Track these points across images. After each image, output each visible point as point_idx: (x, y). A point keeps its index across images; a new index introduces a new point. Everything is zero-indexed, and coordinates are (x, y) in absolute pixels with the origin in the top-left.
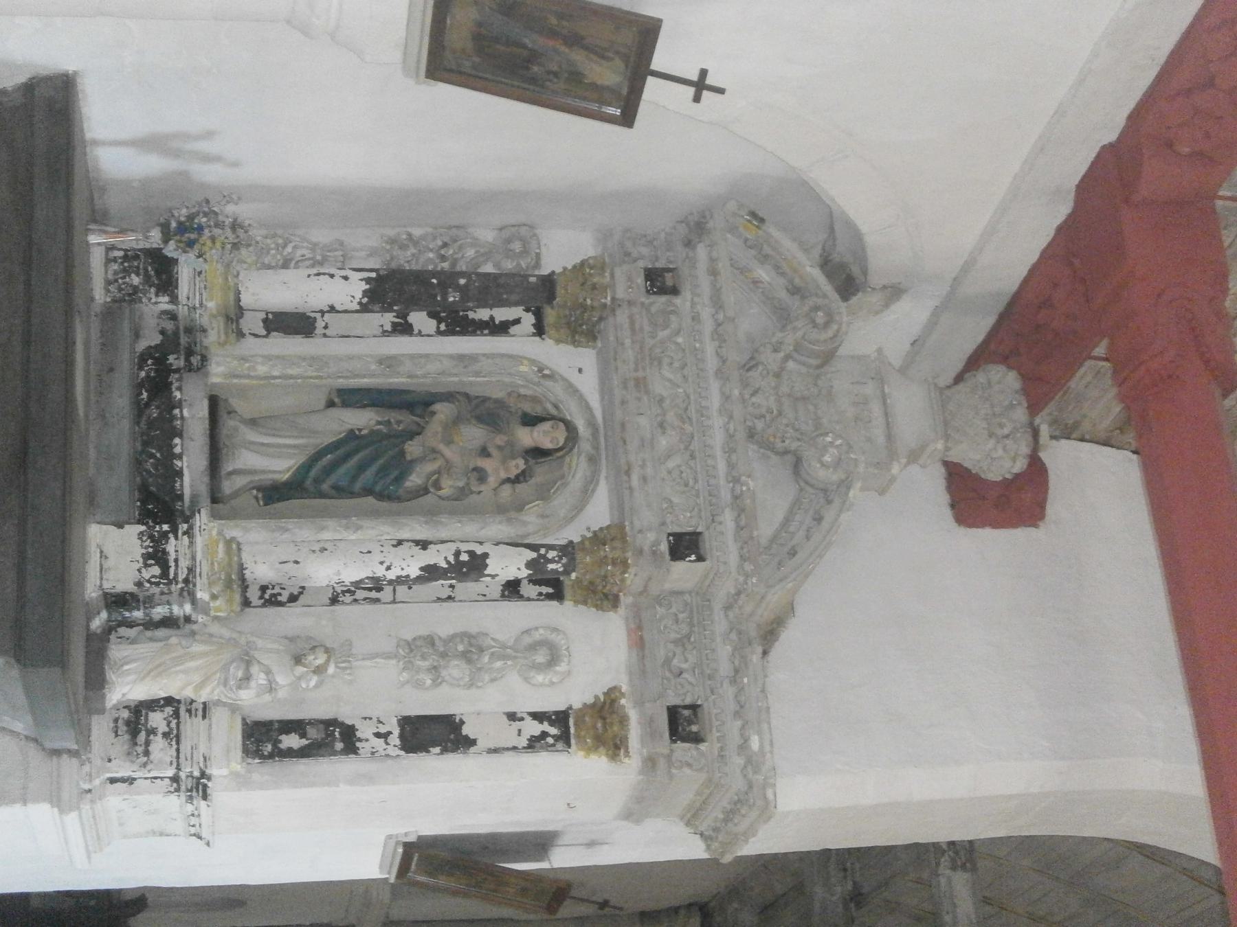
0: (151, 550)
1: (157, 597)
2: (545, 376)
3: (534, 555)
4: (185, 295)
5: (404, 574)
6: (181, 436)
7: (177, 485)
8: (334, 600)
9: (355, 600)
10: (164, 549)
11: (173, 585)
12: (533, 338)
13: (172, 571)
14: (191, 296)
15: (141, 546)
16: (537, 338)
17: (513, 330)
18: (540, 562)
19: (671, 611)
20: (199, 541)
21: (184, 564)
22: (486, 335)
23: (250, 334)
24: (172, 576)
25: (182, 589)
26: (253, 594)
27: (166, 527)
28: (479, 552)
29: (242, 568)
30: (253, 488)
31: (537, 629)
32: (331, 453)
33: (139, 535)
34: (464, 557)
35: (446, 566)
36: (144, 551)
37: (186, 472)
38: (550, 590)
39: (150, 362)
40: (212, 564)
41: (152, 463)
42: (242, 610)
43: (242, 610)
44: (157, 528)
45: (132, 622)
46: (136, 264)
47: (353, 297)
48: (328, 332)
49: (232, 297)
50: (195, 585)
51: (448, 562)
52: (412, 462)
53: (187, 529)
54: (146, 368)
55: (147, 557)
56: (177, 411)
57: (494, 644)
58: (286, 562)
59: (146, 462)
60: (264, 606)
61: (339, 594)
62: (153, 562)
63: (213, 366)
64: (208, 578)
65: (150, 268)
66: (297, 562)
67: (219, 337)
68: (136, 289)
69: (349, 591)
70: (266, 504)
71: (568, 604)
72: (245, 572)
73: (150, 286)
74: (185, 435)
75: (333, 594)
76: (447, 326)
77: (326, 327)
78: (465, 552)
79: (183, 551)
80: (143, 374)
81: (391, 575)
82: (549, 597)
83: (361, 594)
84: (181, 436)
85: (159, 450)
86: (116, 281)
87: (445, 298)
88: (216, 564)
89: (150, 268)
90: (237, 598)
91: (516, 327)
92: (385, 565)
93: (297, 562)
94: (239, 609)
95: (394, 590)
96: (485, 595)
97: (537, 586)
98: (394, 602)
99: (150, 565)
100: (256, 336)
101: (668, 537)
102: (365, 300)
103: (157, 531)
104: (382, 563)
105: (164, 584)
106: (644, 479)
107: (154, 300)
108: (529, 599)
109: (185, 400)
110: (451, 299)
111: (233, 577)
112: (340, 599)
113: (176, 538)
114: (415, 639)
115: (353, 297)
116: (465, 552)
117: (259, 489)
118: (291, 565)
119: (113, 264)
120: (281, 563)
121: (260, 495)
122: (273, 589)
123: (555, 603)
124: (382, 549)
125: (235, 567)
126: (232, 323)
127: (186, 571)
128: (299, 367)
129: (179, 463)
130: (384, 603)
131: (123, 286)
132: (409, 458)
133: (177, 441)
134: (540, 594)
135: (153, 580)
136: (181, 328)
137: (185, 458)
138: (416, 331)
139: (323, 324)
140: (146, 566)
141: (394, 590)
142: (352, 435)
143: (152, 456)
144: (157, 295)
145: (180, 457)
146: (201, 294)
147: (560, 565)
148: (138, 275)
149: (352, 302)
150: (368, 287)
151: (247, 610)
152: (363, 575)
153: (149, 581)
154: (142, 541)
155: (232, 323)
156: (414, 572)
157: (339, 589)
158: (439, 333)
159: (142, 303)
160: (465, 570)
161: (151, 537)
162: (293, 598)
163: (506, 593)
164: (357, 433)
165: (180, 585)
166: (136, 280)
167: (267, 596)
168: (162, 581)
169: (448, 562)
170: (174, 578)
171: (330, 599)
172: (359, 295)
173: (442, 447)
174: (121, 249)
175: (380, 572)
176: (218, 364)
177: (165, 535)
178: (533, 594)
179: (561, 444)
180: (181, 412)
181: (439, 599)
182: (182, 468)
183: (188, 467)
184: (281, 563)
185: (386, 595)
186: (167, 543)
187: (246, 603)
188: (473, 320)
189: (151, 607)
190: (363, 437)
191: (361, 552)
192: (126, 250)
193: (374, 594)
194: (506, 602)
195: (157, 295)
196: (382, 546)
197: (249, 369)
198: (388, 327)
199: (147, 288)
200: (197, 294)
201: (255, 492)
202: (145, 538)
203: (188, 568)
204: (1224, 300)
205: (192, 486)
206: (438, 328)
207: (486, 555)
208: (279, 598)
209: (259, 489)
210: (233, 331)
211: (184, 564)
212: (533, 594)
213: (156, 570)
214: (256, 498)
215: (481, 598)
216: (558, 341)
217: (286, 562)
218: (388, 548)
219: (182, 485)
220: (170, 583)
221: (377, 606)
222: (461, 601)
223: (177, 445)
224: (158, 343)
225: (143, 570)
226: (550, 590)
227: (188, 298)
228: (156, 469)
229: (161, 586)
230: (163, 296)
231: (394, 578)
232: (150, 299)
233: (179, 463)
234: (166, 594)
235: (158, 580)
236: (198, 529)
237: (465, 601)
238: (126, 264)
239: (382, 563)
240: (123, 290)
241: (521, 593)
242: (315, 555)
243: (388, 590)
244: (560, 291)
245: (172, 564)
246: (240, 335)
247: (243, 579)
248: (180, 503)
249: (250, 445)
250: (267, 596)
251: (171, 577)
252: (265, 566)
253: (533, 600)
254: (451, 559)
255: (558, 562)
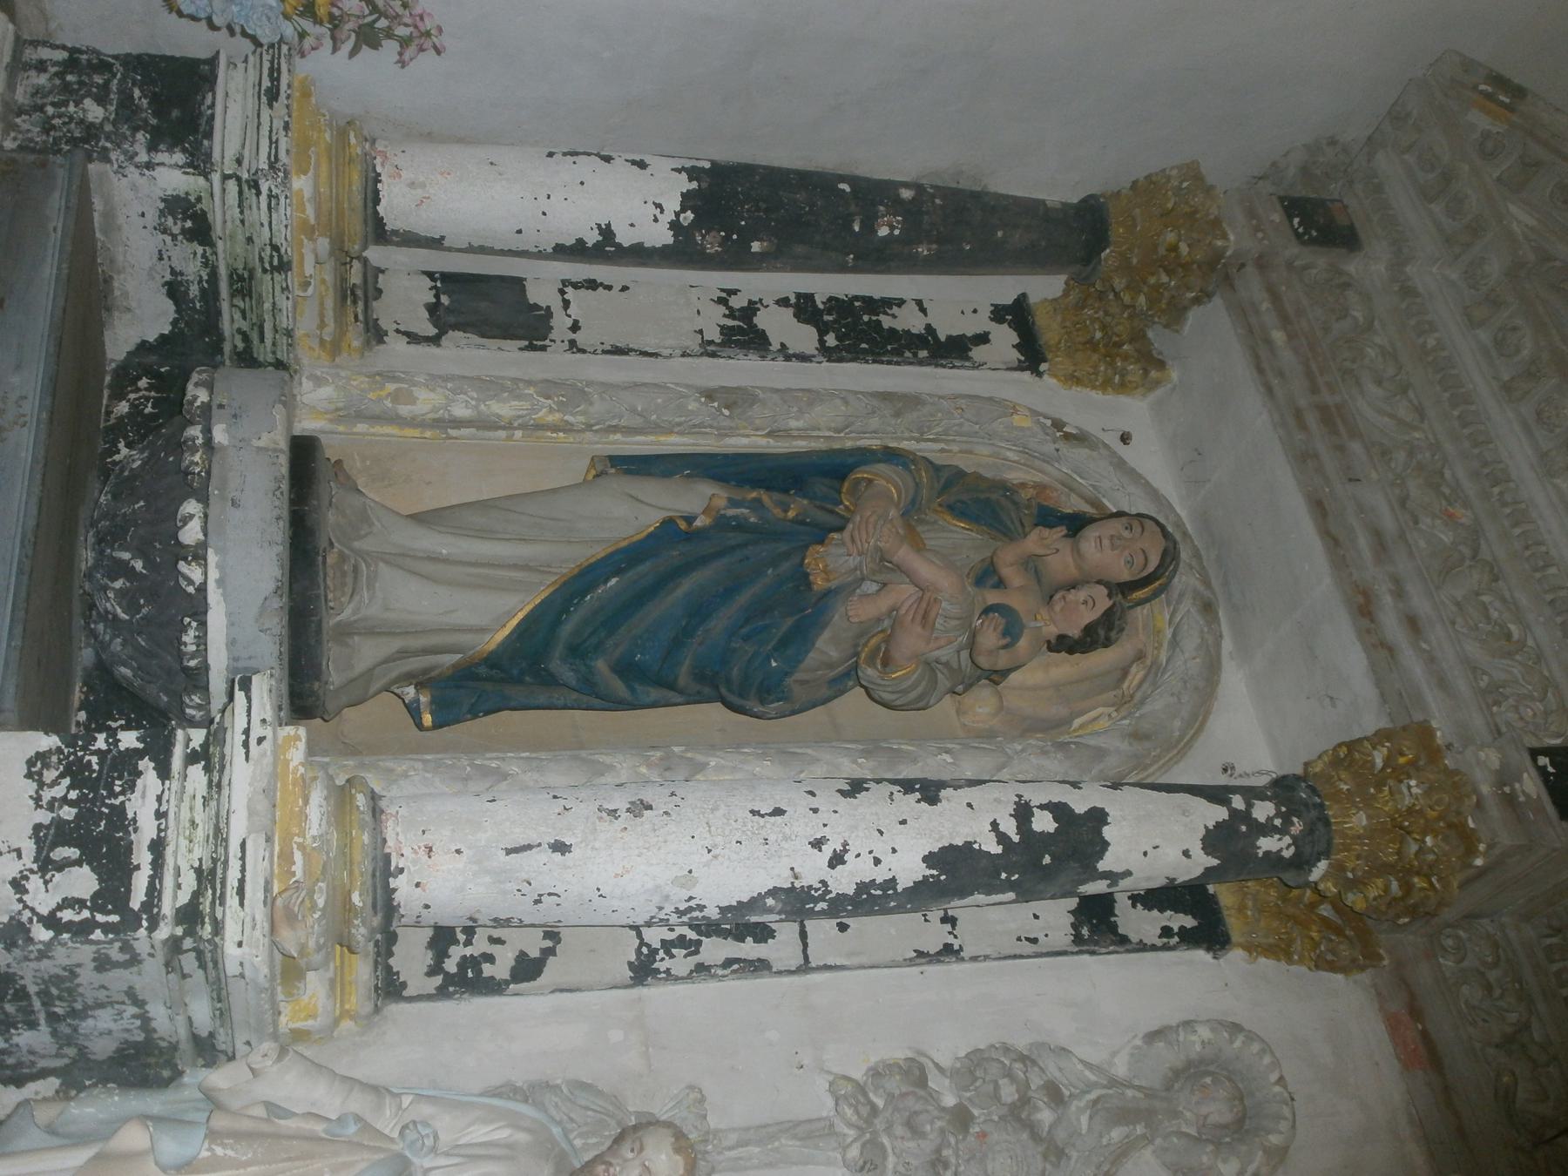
0: (68, 813)
1: (87, 976)
2: (1067, 436)
3: (1221, 813)
4: (231, 153)
5: (880, 875)
6: (204, 500)
7: (189, 637)
8: (643, 970)
9: (701, 968)
10: (120, 811)
11: (142, 932)
12: (1017, 374)
13: (140, 882)
14: (246, 153)
15: (37, 800)
16: (1026, 375)
17: (977, 353)
18: (1237, 831)
19: (1465, 964)
20: (242, 776)
21: (185, 856)
22: (921, 363)
23: (398, 331)
24: (137, 898)
25: (174, 945)
26: (411, 958)
27: (129, 740)
28: (1080, 808)
29: (384, 870)
30: (408, 678)
31: (1188, 1024)
32: (618, 572)
33: (31, 763)
34: (1044, 823)
35: (998, 850)
36: (44, 817)
37: (214, 596)
38: (1189, 922)
39: (143, 383)
40: (286, 858)
41: (121, 593)
42: (377, 1010)
43: (377, 1010)
44: (101, 742)
45: (20, 1064)
46: (98, 79)
47: (658, 206)
48: (579, 337)
49: (356, 179)
50: (218, 928)
51: (1002, 838)
52: (828, 593)
53: (205, 745)
54: (132, 396)
55: (48, 838)
56: (195, 432)
57: (1093, 1078)
58: (529, 847)
59: (105, 588)
60: (442, 993)
61: (656, 951)
62: (73, 853)
63: (307, 384)
64: (270, 901)
65: (137, 93)
66: (560, 847)
67: (322, 325)
68: (91, 132)
69: (682, 942)
70: (437, 725)
71: (1236, 955)
72: (393, 883)
73: (135, 129)
74: (214, 492)
75: (639, 951)
76: (837, 338)
77: (575, 327)
78: (1042, 807)
79: (185, 814)
80: (123, 408)
81: (843, 882)
82: (1189, 938)
83: (715, 950)
84: (204, 500)
85: (140, 552)
86: (41, 109)
87: (869, 226)
88: (298, 856)
89: (137, 93)
90: (362, 971)
91: (983, 348)
92: (828, 850)
93: (560, 847)
94: (368, 1007)
95: (803, 935)
96: (1034, 941)
97: (1155, 912)
98: (805, 967)
99: (61, 866)
100: (413, 338)
101: (1534, 760)
102: (688, 217)
103: (98, 752)
104: (818, 844)
105: (106, 928)
106: (1413, 624)
107: (143, 157)
108: (1142, 947)
109: (221, 406)
110: (883, 232)
111: (356, 898)
112: (662, 966)
113: (164, 772)
114: (876, 1073)
115: (658, 206)
116: (1042, 807)
117: (422, 680)
118: (544, 856)
119: (33, 73)
120: (509, 852)
121: (424, 699)
122: (468, 943)
123: (1201, 955)
124: (815, 802)
125: (363, 865)
126: (355, 302)
127: (189, 882)
128: (519, 397)
129: (195, 573)
130: (780, 973)
131: (56, 121)
132: (819, 583)
133: (191, 507)
134: (1166, 932)
135: (67, 915)
136: (223, 272)
137: (212, 557)
138: (775, 346)
139: (569, 322)
140: (46, 865)
141: (803, 935)
142: (670, 532)
143: (125, 570)
144: (152, 147)
145: (198, 554)
146: (274, 143)
147: (1287, 840)
148: (101, 100)
149: (656, 220)
150: (694, 185)
151: (395, 1009)
152: (762, 884)
153: (51, 921)
154: (41, 785)
155: (355, 302)
156: (909, 868)
157: (654, 936)
158: (828, 353)
159: (109, 161)
160: (1047, 860)
161: (75, 772)
162: (527, 969)
163: (1085, 931)
164: (683, 525)
165: (163, 932)
166: (94, 112)
167: (451, 966)
168: (100, 918)
169: (1002, 838)
170: (148, 906)
171: (630, 964)
172: (673, 204)
173: (904, 554)
174: (64, 47)
175: (813, 870)
176: (319, 382)
177: (124, 766)
178: (1151, 934)
179: (1151, 568)
180: (207, 431)
181: (920, 954)
182: (202, 589)
183: (220, 582)
184: (509, 852)
185: (782, 947)
186: (130, 787)
187: (390, 988)
188: (892, 331)
189: (73, 1013)
190: (700, 534)
191: (753, 812)
192: (73, 51)
193: (749, 949)
194: (1086, 957)
195: (152, 147)
196: (812, 794)
197: (396, 397)
198: (714, 335)
199: (125, 129)
200: (265, 143)
201: (410, 692)
202: (50, 775)
203: (199, 871)
204: (139, 1042)
205: (231, 643)
206: (822, 342)
207: (1098, 817)
208: (487, 970)
209: (422, 680)
210: (356, 317)
211: (185, 856)
212: (1151, 934)
213: (83, 882)
214: (413, 710)
215: (1029, 948)
216: (1073, 379)
217: (529, 847)
218: (827, 799)
219: (202, 640)
220: (130, 921)
221: (764, 983)
222: (974, 959)
223: (191, 517)
224: (166, 330)
225: (34, 883)
226: (1189, 922)
227: (239, 162)
228: (132, 608)
229: (98, 935)
230: (170, 150)
231: (851, 891)
232: (131, 157)
233: (195, 573)
234: (117, 965)
235: (86, 914)
236: (240, 738)
237: (986, 957)
238: (69, 78)
239: (818, 844)
240: (53, 127)
241: (1121, 931)
242: (619, 824)
243: (787, 932)
244: (1117, 231)
245: (143, 857)
246: (375, 334)
247: (387, 906)
248: (196, 699)
249: (402, 560)
250: (451, 966)
251: (135, 904)
252: (460, 863)
253: (1154, 948)
254: (1009, 827)
255: (1283, 831)
